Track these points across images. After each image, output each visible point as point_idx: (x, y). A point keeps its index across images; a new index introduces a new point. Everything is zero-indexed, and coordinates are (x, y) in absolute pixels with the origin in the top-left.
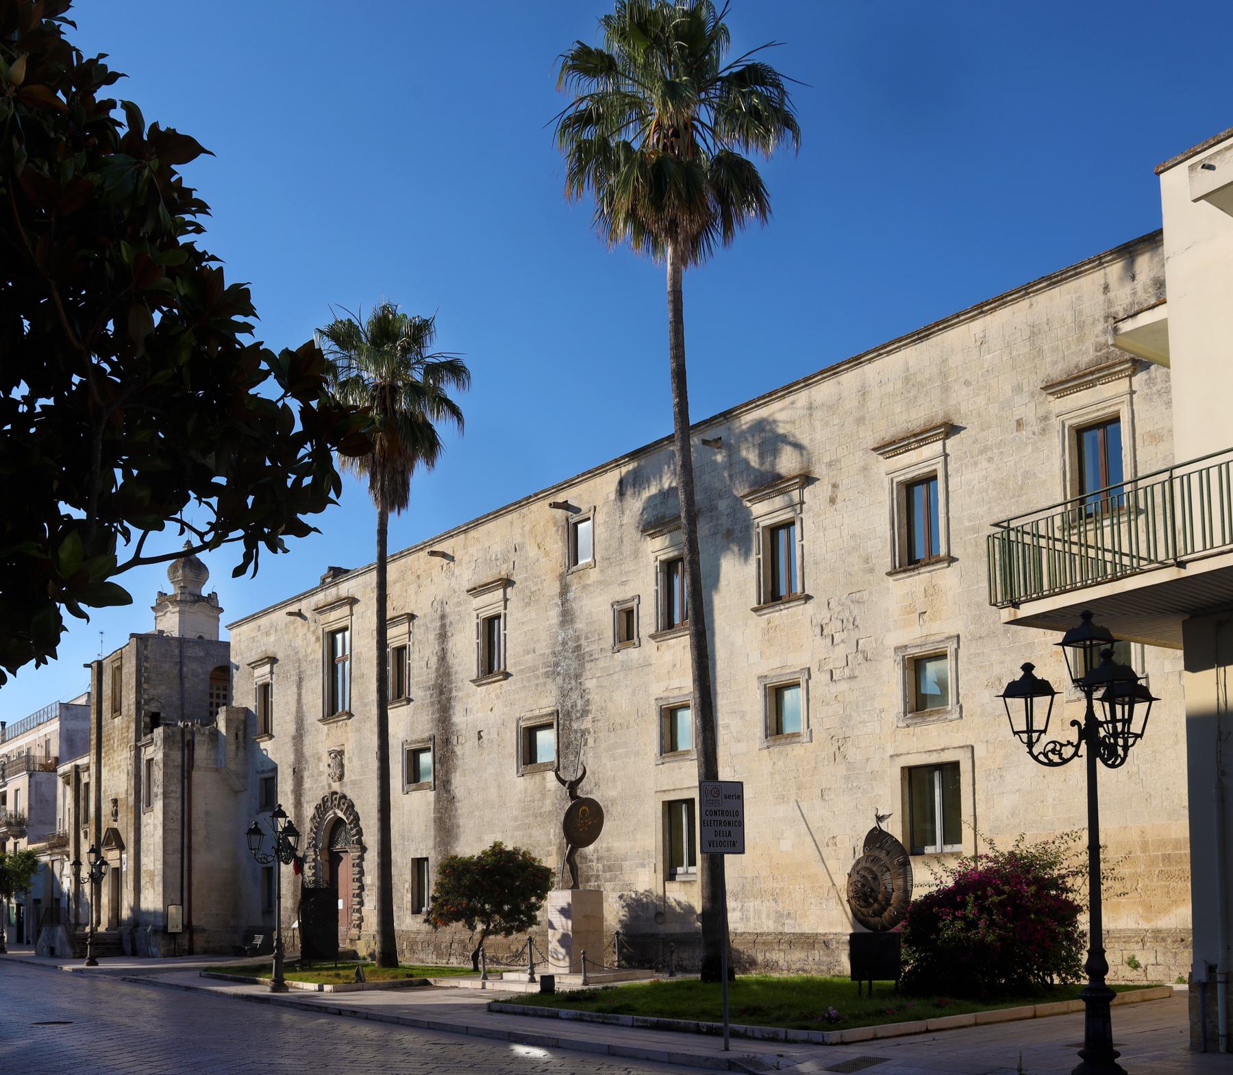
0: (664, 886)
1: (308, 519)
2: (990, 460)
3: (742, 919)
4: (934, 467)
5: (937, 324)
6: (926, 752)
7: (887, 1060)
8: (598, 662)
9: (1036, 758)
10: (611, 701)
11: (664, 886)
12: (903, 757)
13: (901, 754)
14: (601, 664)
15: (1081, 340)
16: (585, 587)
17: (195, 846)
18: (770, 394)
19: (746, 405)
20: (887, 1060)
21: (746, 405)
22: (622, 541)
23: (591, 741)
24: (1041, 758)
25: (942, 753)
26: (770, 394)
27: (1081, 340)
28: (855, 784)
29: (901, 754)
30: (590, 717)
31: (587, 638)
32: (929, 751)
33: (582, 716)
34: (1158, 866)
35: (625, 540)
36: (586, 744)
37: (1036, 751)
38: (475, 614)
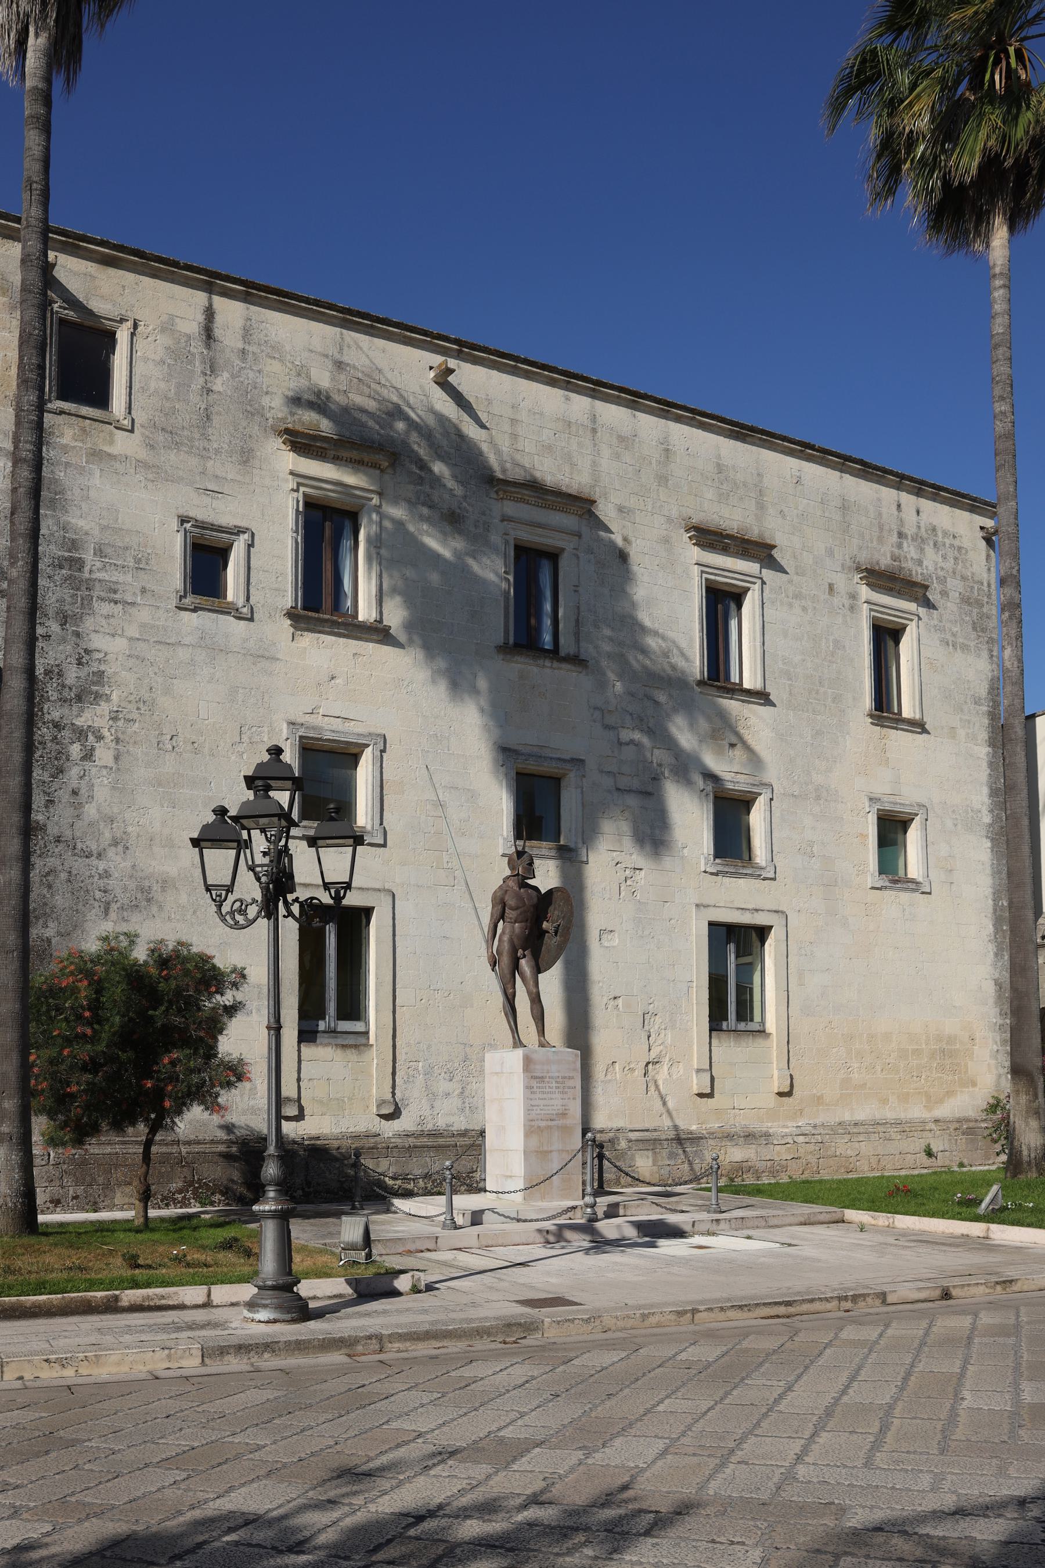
0: (299, 1051)
1: (884, 160)
2: (804, 609)
3: (463, 1110)
4: (748, 585)
5: (784, 439)
6: (738, 909)
7: (517, 1302)
8: (133, 610)
9: (223, 920)
10: (167, 691)
11: (299, 1051)
12: (711, 909)
13: (708, 906)
14: (144, 615)
15: (881, 539)
16: (96, 455)
17: (364, 816)
18: (544, 367)
19: (503, 355)
20: (517, 1302)
21: (503, 355)
22: (208, 417)
23: (104, 755)
24: (228, 918)
25: (756, 914)
26: (544, 367)
27: (881, 539)
28: (646, 933)
29: (708, 906)
30: (104, 708)
31: (99, 552)
32: (742, 909)
33: (79, 698)
34: (936, 1059)
35: (216, 420)
36: (88, 755)
37: (226, 908)
38: (291, 483)
